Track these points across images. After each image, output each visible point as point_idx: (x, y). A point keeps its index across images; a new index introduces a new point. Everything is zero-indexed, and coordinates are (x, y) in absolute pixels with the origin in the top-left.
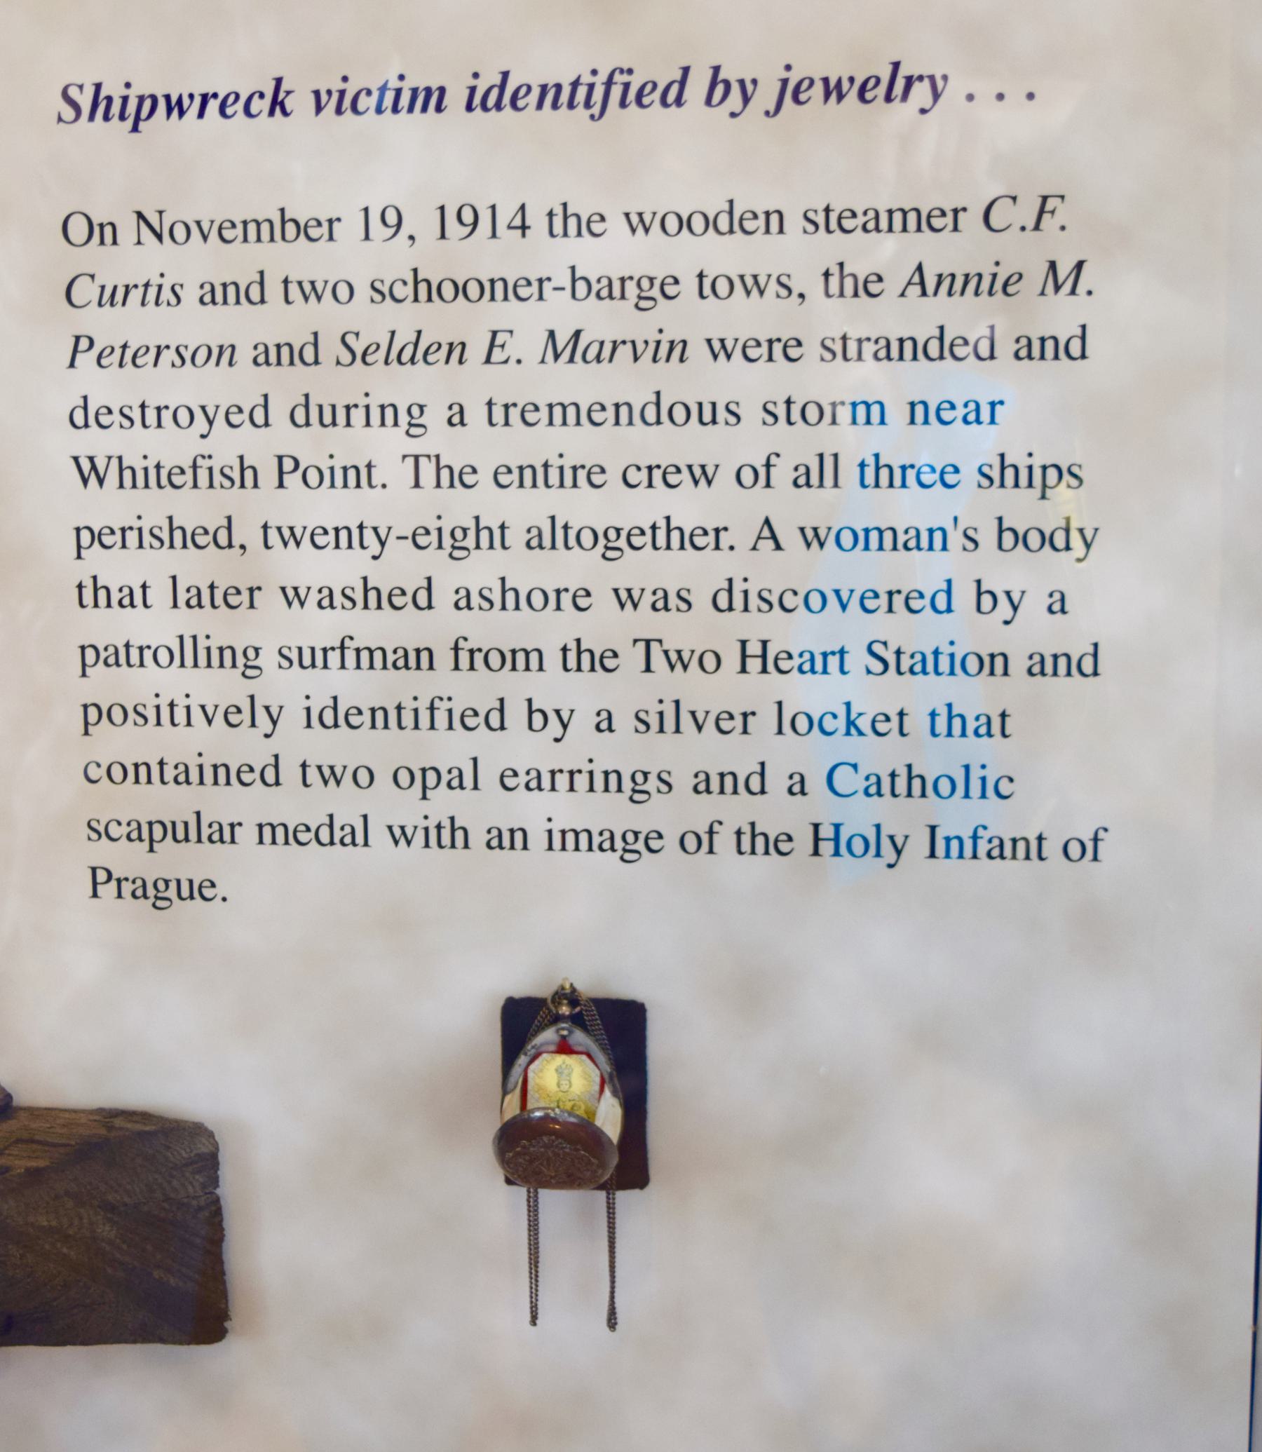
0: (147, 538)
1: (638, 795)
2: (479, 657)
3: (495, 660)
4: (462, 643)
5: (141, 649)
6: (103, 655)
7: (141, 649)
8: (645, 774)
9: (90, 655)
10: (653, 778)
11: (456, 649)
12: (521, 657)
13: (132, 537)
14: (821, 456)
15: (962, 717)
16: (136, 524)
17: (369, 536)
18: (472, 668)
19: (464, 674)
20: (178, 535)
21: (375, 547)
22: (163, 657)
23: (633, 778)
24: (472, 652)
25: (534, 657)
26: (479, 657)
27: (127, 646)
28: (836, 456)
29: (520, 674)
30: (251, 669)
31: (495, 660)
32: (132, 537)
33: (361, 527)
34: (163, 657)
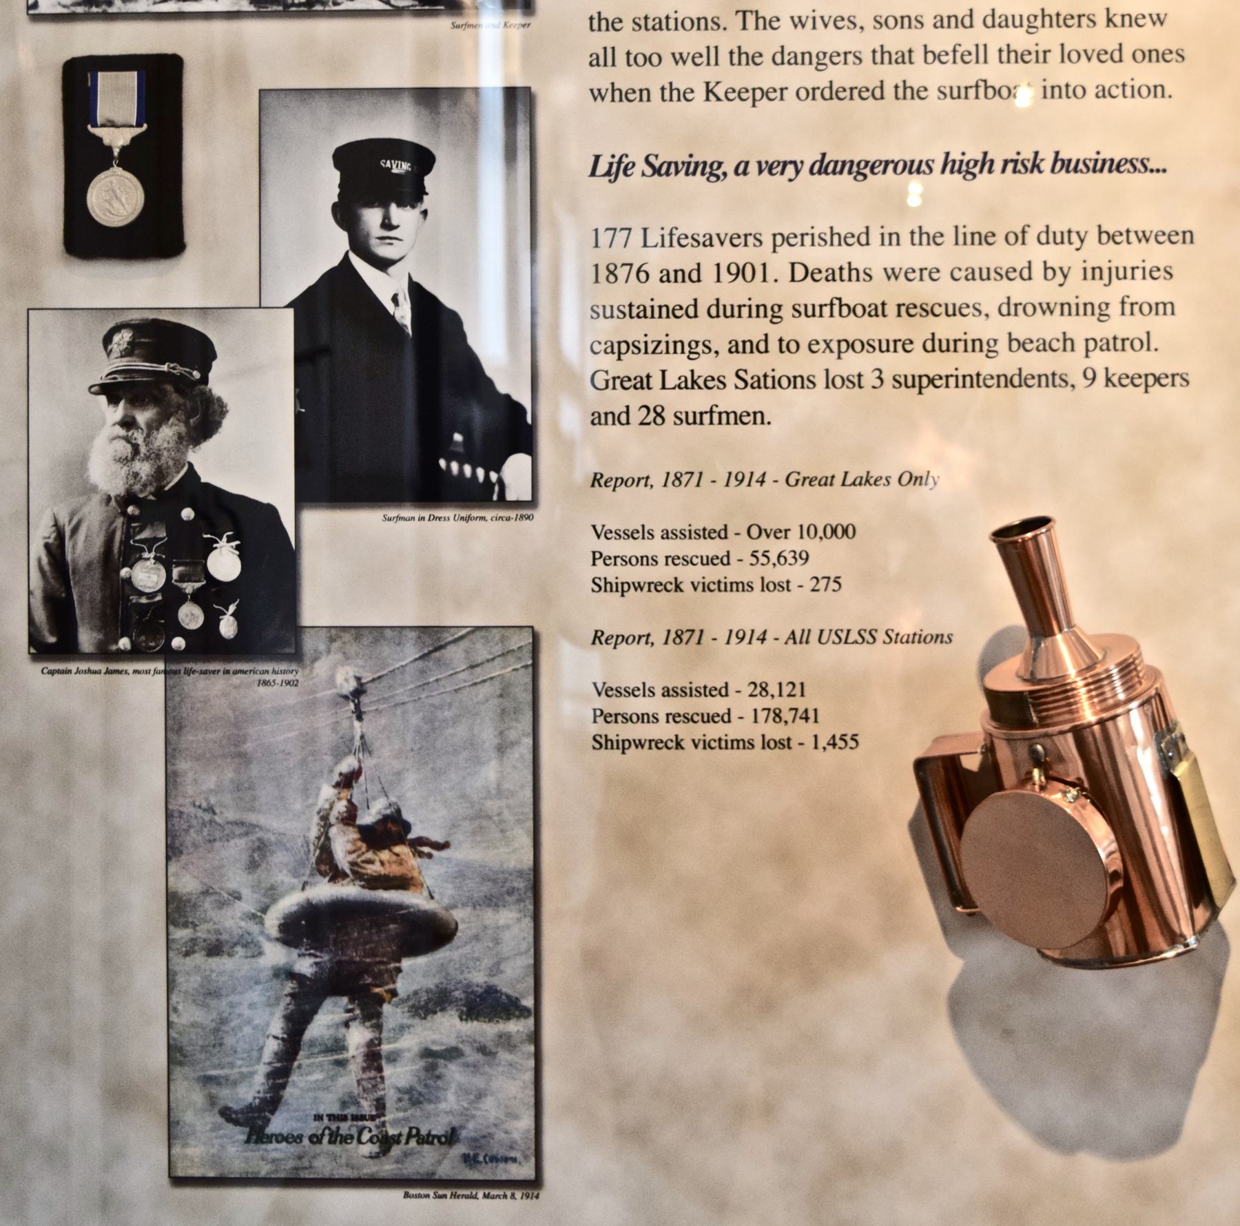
0: (817, 240)
1: (692, 355)
2: (1136, 308)
3: (1146, 309)
4: (1126, 300)
5: (1123, 340)
6: (1099, 344)
7: (1123, 340)
8: (697, 343)
9: (1091, 344)
10: (700, 344)
11: (1123, 303)
12: (1161, 307)
13: (808, 239)
14: (605, 49)
15: (857, 270)
16: (811, 231)
17: (1074, 237)
18: (1132, 314)
19: (1128, 318)
20: (836, 238)
21: (1077, 243)
22: (1137, 344)
23: (690, 345)
24: (1132, 304)
25: (1169, 307)
26: (1136, 308)
27: (1115, 338)
28: (613, 48)
29: (1161, 318)
30: (776, 318)
31: (1146, 309)
32: (808, 239)
33: (1069, 232)
34: (1137, 344)
